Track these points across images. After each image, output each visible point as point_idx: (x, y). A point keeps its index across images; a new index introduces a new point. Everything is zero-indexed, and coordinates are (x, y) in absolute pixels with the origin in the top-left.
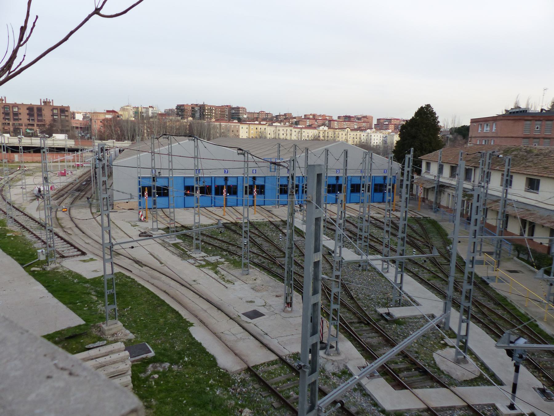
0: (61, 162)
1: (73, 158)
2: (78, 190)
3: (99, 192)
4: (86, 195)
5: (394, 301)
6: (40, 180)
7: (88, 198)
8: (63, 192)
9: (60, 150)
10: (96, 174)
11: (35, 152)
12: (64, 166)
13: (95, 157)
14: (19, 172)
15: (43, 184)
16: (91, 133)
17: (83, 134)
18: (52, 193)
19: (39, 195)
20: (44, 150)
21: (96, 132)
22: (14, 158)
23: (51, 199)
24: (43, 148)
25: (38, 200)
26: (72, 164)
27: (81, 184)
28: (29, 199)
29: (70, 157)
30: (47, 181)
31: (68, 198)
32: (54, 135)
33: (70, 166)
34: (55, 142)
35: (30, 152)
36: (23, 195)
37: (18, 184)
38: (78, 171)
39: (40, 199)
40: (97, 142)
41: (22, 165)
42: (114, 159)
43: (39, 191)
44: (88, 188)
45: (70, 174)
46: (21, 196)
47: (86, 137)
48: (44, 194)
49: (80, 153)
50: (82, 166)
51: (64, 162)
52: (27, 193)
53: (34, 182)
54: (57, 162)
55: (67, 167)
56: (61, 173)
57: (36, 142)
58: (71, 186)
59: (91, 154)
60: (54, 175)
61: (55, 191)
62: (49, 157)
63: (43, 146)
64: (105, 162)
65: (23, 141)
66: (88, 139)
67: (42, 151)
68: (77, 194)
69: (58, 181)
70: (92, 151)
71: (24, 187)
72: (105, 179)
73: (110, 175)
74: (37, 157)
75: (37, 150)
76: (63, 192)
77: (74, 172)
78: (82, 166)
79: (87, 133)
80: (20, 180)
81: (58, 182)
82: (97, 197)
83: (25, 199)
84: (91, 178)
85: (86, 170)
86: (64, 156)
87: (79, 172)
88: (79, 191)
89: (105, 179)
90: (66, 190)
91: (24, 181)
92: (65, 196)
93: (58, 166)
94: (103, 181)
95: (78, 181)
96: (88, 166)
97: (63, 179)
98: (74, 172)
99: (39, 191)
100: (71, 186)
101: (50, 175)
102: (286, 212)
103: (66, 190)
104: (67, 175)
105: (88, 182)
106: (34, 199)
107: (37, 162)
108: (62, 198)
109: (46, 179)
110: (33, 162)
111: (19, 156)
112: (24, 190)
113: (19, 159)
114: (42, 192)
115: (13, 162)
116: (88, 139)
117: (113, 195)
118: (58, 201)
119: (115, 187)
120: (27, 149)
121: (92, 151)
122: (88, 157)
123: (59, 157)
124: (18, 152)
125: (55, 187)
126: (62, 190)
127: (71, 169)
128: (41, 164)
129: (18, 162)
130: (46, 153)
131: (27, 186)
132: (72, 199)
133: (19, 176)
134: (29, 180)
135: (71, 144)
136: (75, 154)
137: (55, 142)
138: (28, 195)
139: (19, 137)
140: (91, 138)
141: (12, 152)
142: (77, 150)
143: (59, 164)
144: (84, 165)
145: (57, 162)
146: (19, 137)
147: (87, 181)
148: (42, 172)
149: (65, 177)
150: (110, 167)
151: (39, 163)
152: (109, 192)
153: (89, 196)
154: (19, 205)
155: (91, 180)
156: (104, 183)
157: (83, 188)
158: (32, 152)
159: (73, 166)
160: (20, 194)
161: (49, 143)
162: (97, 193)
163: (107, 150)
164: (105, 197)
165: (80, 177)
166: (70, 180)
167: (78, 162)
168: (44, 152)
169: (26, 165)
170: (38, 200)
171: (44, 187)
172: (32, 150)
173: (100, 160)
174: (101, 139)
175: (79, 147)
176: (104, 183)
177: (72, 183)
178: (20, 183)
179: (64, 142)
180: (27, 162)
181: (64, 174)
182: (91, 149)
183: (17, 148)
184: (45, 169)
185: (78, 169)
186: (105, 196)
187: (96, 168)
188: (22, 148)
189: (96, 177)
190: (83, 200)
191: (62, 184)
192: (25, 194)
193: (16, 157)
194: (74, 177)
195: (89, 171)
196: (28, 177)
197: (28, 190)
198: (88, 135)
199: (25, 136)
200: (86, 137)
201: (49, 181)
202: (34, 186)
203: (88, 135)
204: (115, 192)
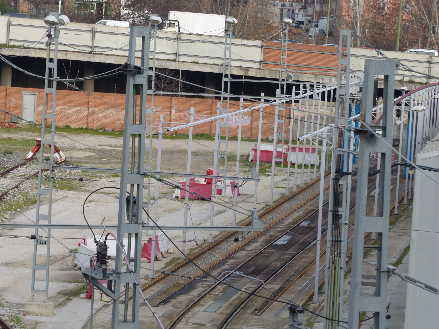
0: (197, 136)
1: (246, 121)
2: (255, 268)
3: (344, 285)
4: (287, 296)
5: (152, 117)
6: (108, 209)
7: (293, 311)
8: (191, 272)
9: (198, 83)
10: (337, 202)
11: (102, 86)
12: (207, 155)
13: (342, 122)
14: (30, 169)
15: (119, 227)
16: (336, 13)
17: (301, 17)
18: (148, 269)
19: (98, 275)
20: (141, 80)
21: (360, 9)
22: (20, 106)
23: (142, 296)
24: (138, 71)
25: (90, 297)
26: (240, 148)
27: (270, 244)
28: (55, 287)
29: (235, 115)
30: (134, 217)
31: (209, 302)
32: (173, 15)
33: (232, 158)
34: (184, 48)
35: (81, 86)
36: (35, 267)
37: (21, 219)
38: (265, 181)
39: (97, 294)
40: (359, 58)
41: (46, 138)
42: (426, 139)
43: (102, 256)
44: (299, 264)
45: (228, 192)
46: (28, 272)
47: (313, 31)
48: (117, 273)
49: (280, 98)
50: (283, 161)
51: (209, 137)
52: (50, 261)
53: (81, 217)
54: (181, 135)
55: (222, 161)
56: (193, 184)
57: (111, 40)
58: (231, 246)
59: (325, 109)
60: (164, 195)
61: (159, 266)
62: (158, 111)
63: (138, 63)
64: (384, 145)
65: (65, 37)
66: (321, 38)
67: (130, 83)
68: (248, 284)
69: (176, 219)
70: (330, 96)
71: (42, 233)
72: (378, 224)
73: (402, 210)
74: (109, 109)
75: (111, 78)
76: (191, 272)
77: (247, 188)
78: (283, 161)
79: (321, 14)
80: (33, 202)
81: (179, 224)
82: (334, 306)
83: (40, 285)
84: (312, 216)
85: (300, 178)
86: (212, 113)
87: (265, 188)
88: (255, 273)
89: (378, 224)
90: (204, 263)
91: (44, 209)
92: (199, 289)
93: (184, 152)
94: (368, 236)
95: (258, 224)
96: (309, 163)
97: (199, 211)
98: (247, 188)
99: (102, 256)
100: (231, 246)
101: (152, 187)
102: (146, 178)
103: (204, 263)
104: (215, 197)
105: (302, 236)
106: (74, 294)
107: (102, 131)
108: (183, 298)
109: (131, 205)
110: (87, 130)
111: (38, 102)
112: (42, 250)
113: (36, 113)
114: (111, 265)
115: (13, 125)
116: (321, 38)
117: (402, 308)
118: (168, 308)
119: (415, 266)
120: (75, 72)
121: (330, 96)
122: (314, 120)
123: (191, 114)
124: (39, 84)
125: (164, 246)
126: (190, 260)
127: (237, 170)
128: (119, 141)
129: (33, 127)
130: (145, 91)
131: (55, 232)
132: (224, 308)
133: (27, 185)
134: (66, 207)
135: (247, 57)
136: (262, 105)
137: (184, 48)
138: (54, 271)
139: (51, 18)
140: (332, 35)
141: (20, 81)
142: (269, 88)
143: (191, 145)
144: (292, 157)
145: (181, 135)
146: (51, 18)
147: (294, 229)
148: (120, 173)
149: (206, 205)
150: (404, 170)
151: (112, 134)
152: (390, 284)
153: (300, 303)
154: (14, 311)
155: (312, 229)
156: (374, 243)
157: (274, 260)
158: (90, 86)
159: (245, 159)
160: (23, 264)
161: (163, 50)
162: (334, 292)
163: (398, 93)
164: (370, 310)
165: (269, 211)
166: (228, 219)
167: (266, 140)
168: (138, 89)
169: (60, 141)
170: (90, 297)
171: (119, 238)
172: (89, 79)
173: (365, 135)
174: (379, 39)
175: (281, 74)
176: (374, 243)
177: (232, 236)
178: (29, 215)
179: (218, 51)
180: (67, 128)
181: (202, 194)
182: (330, 83)
183: (38, 64)
184: (135, 165)
185: (263, 171)
186: (372, 305)
187: (340, 173)
188: (54, 66)
189: (337, 217)
190: (268, 315)
191: (190, 235)
192: (46, 266)
193: (28, 103)
194: (244, 210)
195: (308, 186)
196: (61, 193)
197: (56, 249)
198: (324, 23)
199: (73, 19)
200: (313, 31)
201: (144, 217)
202: (79, 234)
203: (324, 23)
204: (414, 295)
